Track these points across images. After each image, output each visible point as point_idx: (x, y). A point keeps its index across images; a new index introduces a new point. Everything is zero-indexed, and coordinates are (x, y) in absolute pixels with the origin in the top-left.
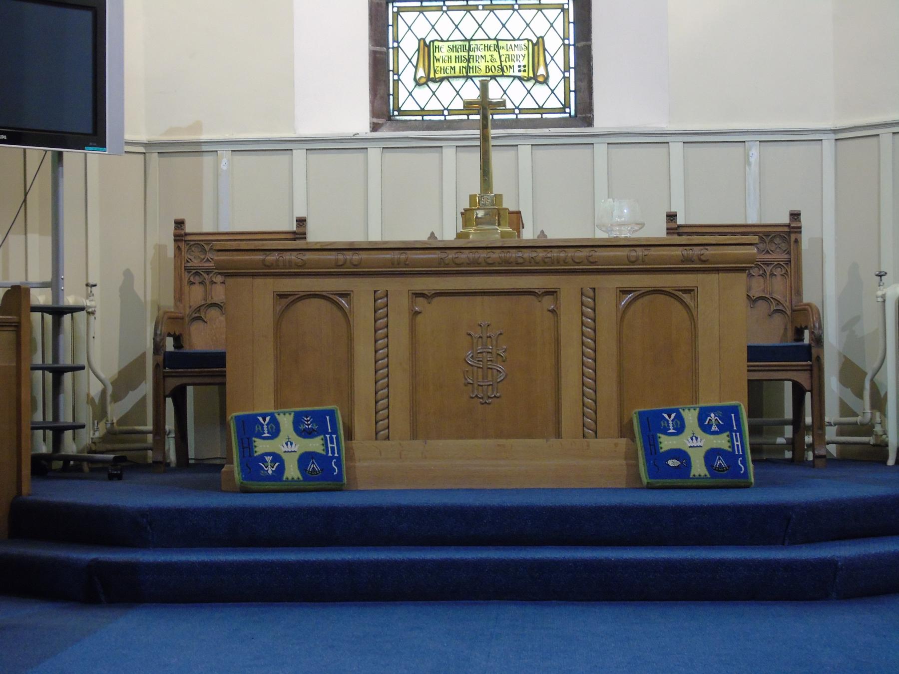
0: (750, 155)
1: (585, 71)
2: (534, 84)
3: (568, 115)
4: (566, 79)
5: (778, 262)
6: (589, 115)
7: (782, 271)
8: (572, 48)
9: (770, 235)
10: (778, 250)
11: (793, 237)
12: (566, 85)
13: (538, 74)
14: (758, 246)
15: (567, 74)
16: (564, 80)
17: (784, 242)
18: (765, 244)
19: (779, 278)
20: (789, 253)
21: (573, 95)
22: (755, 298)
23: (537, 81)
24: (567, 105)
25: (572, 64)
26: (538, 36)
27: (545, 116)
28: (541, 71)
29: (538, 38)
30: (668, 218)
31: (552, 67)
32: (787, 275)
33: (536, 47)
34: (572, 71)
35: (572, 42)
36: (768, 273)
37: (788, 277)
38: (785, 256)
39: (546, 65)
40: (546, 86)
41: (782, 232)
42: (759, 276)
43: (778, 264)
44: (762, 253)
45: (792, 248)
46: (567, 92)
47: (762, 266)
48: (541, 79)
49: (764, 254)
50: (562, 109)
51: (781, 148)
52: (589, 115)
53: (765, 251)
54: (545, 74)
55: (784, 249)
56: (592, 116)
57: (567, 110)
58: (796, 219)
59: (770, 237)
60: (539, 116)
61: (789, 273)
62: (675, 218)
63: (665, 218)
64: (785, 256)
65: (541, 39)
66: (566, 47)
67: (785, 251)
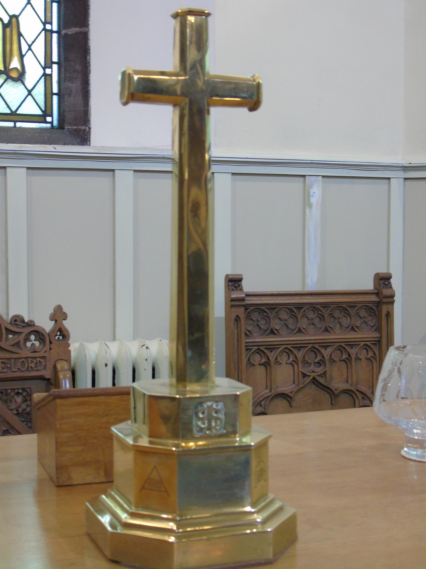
0: (311, 194)
1: (78, 68)
2: (5, 81)
3: (49, 125)
4: (47, 77)
6: (83, 127)
8: (55, 36)
11: (385, 309)
12: (47, 85)
13: (11, 67)
14: (340, 320)
15: (48, 71)
16: (45, 79)
17: (371, 316)
19: (364, 363)
20: (379, 329)
21: (55, 99)
22: (338, 391)
23: (9, 78)
24: (48, 112)
25: (55, 58)
26: (11, 14)
27: (19, 125)
28: (15, 63)
29: (11, 17)
30: (230, 284)
31: (29, 59)
32: (375, 359)
33: (8, 30)
34: (55, 67)
35: (55, 28)
36: (353, 357)
37: (376, 361)
38: (374, 335)
39: (22, 57)
40: (23, 86)
46: (49, 96)
47: (346, 348)
48: (14, 75)
50: (41, 117)
51: (345, 185)
52: (83, 127)
54: (19, 67)
55: (372, 325)
56: (87, 129)
57: (49, 119)
59: (357, 308)
60: (11, 124)
61: (378, 356)
64: (374, 335)
65: (14, 20)
66: (49, 33)
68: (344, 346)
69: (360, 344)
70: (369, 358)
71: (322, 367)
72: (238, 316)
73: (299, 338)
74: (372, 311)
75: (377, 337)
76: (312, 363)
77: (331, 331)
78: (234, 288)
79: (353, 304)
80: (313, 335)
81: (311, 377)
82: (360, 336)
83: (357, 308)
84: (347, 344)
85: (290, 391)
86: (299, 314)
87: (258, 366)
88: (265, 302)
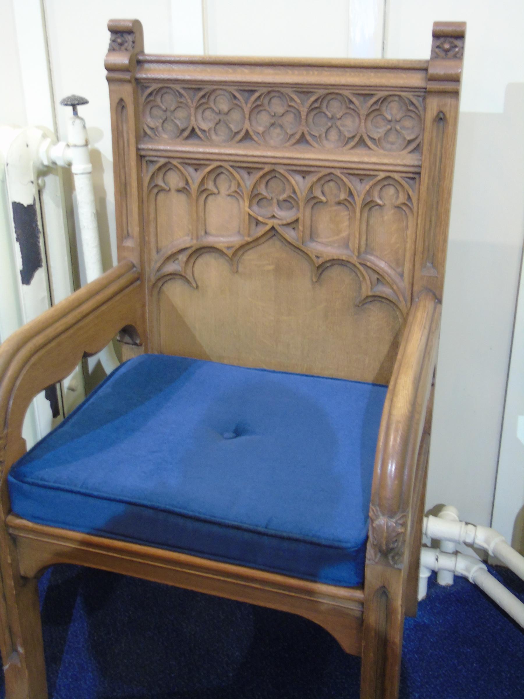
5: (387, 174)
7: (398, 197)
9: (371, 95)
10: (392, 137)
18: (357, 120)
19: (389, 214)
41: (403, 88)
42: (339, 203)
43: (389, 177)
44: (347, 143)
45: (427, 135)
47: (345, 179)
49: (353, 148)
53: (357, 139)
55: (409, 138)
58: (446, 51)
62: (458, 42)
63: (107, 36)
67: (410, 142)
68: (339, 175)
69: (376, 176)
70: (400, 206)
71: (294, 210)
72: (121, 100)
73: (233, 151)
74: (411, 108)
75: (413, 166)
76: (275, 201)
77: (315, 144)
78: (443, 54)
79: (362, 90)
80: (275, 148)
81: (268, 228)
82: (374, 160)
83: (257, 95)
84: (346, 171)
85: (226, 245)
86: (246, 103)
87: (173, 193)
88: (180, 77)
